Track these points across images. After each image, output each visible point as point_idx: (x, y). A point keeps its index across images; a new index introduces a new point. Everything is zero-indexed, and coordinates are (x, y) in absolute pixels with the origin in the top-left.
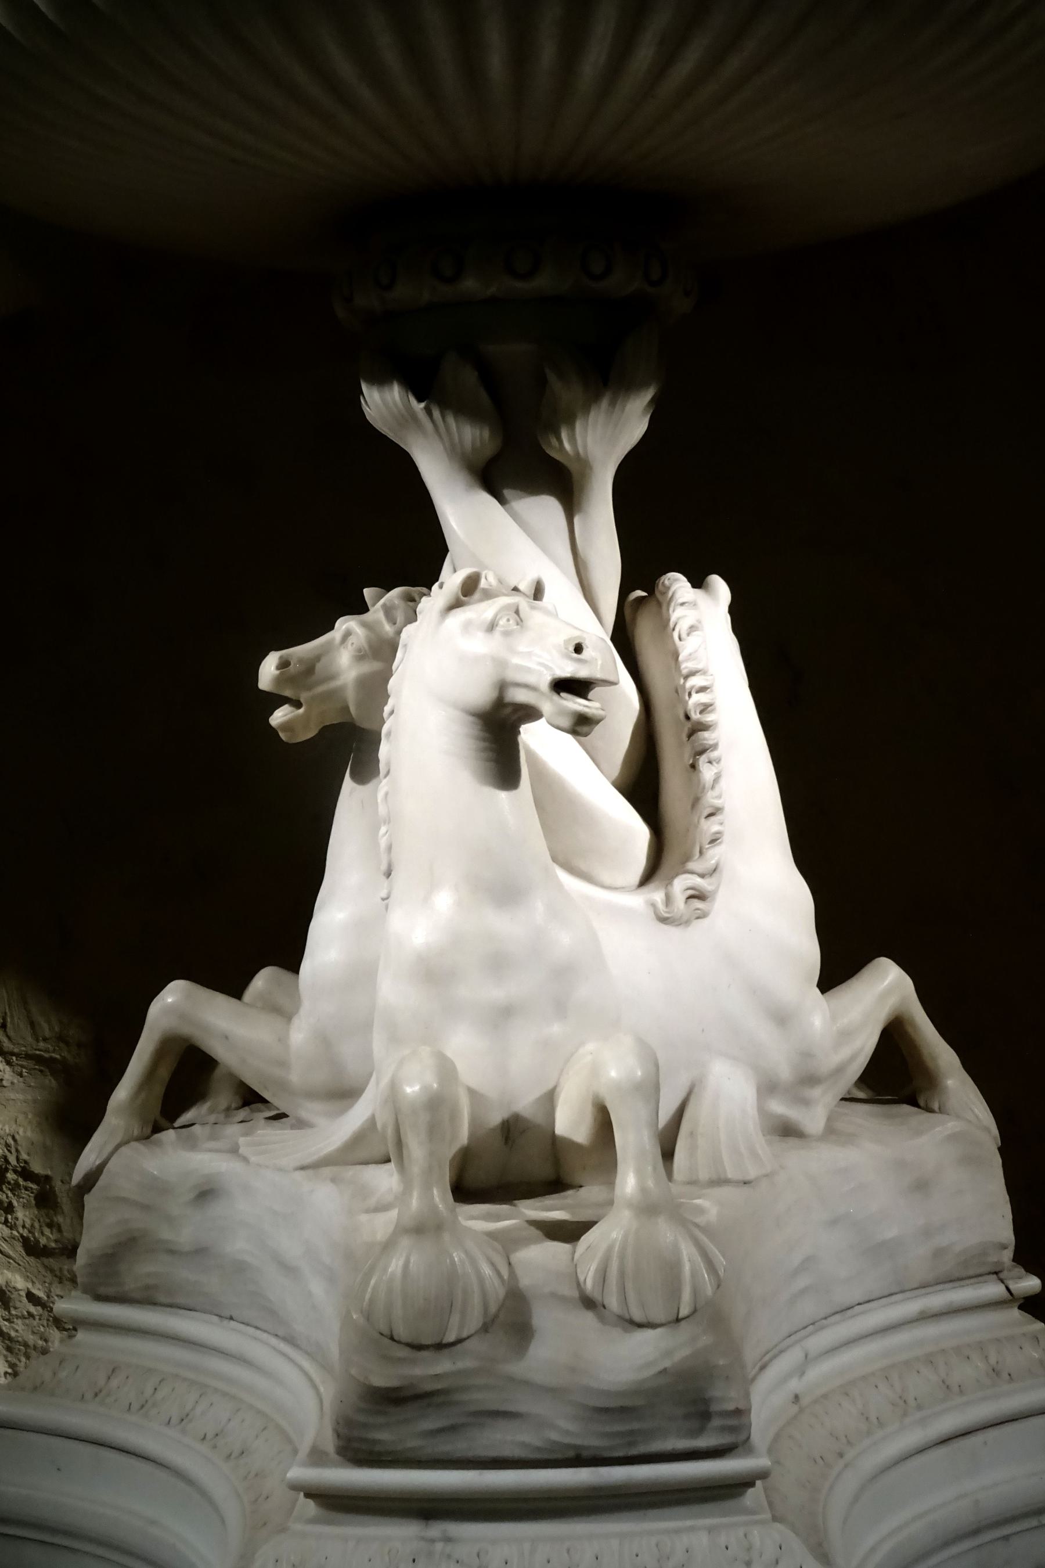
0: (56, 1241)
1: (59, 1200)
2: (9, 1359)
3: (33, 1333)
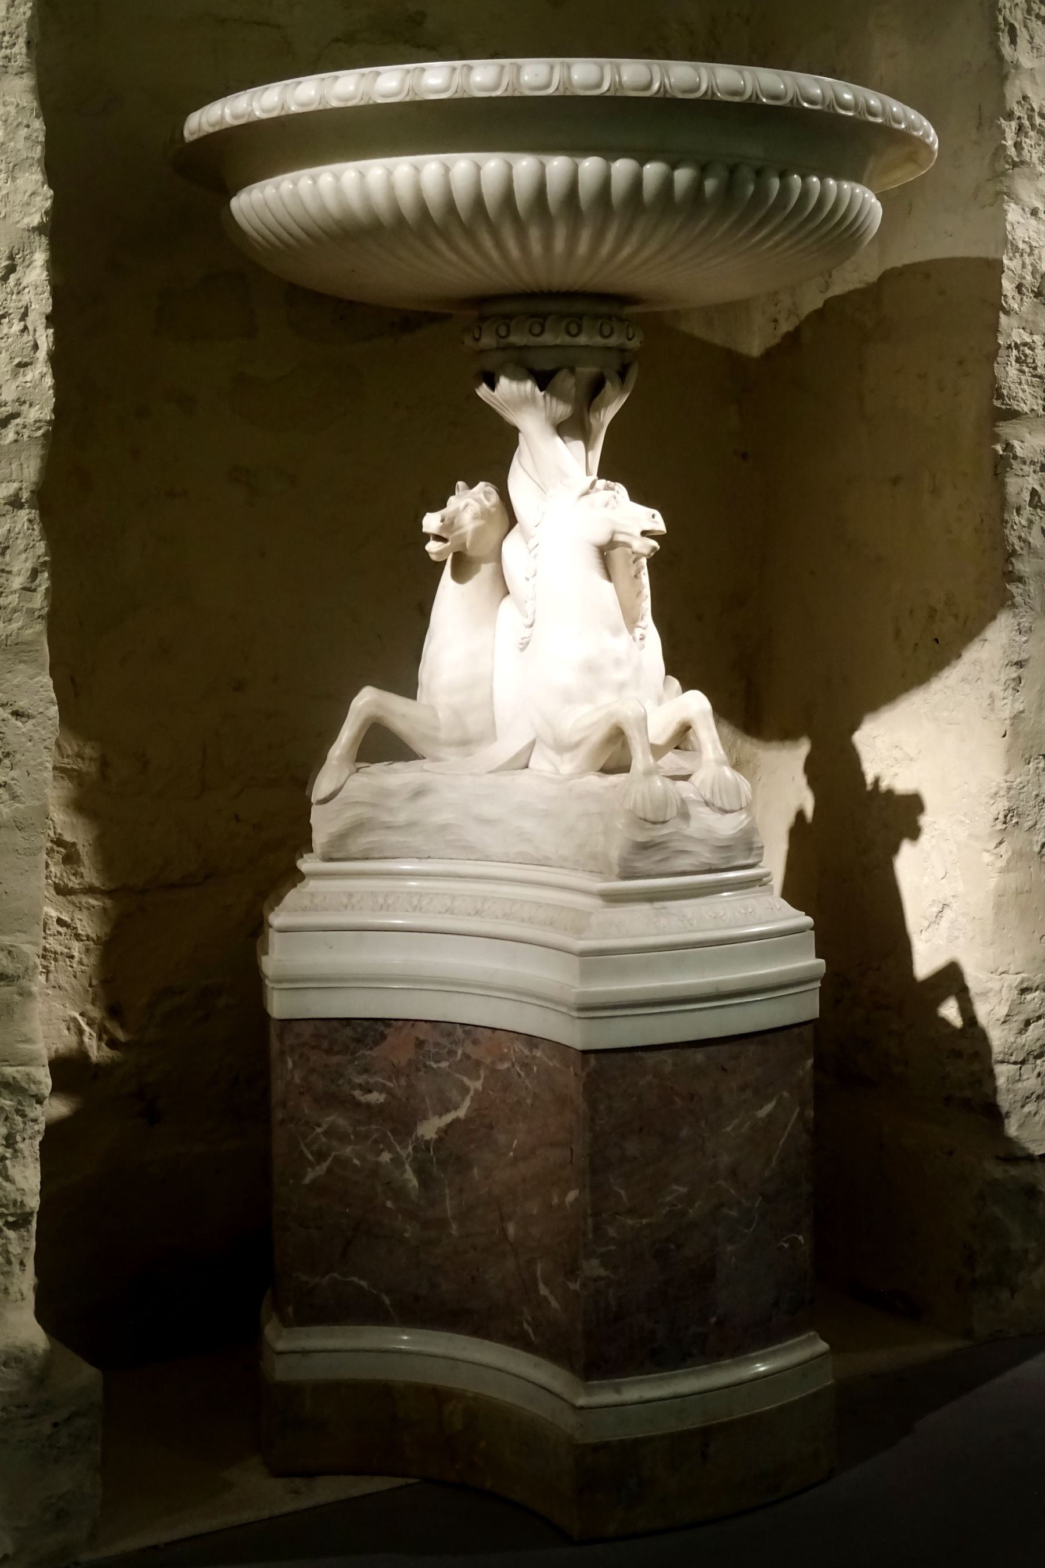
0: (79, 884)
1: (81, 858)
2: (43, 963)
3: (61, 944)
